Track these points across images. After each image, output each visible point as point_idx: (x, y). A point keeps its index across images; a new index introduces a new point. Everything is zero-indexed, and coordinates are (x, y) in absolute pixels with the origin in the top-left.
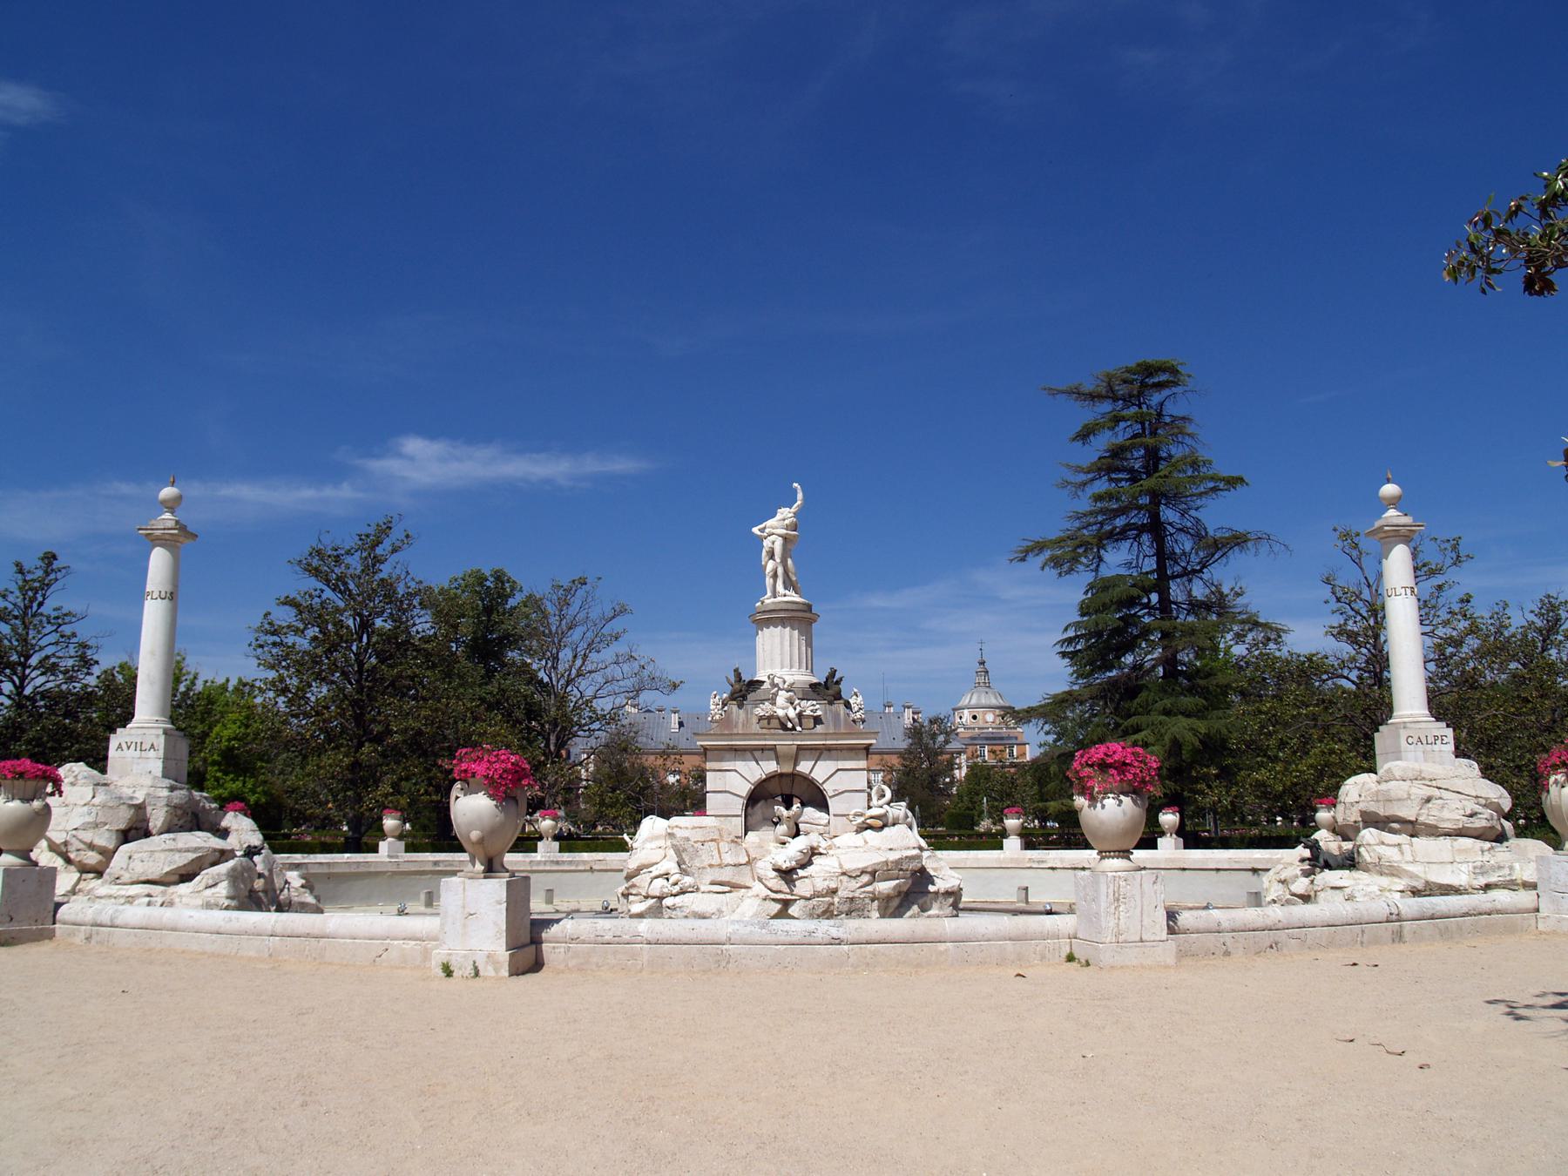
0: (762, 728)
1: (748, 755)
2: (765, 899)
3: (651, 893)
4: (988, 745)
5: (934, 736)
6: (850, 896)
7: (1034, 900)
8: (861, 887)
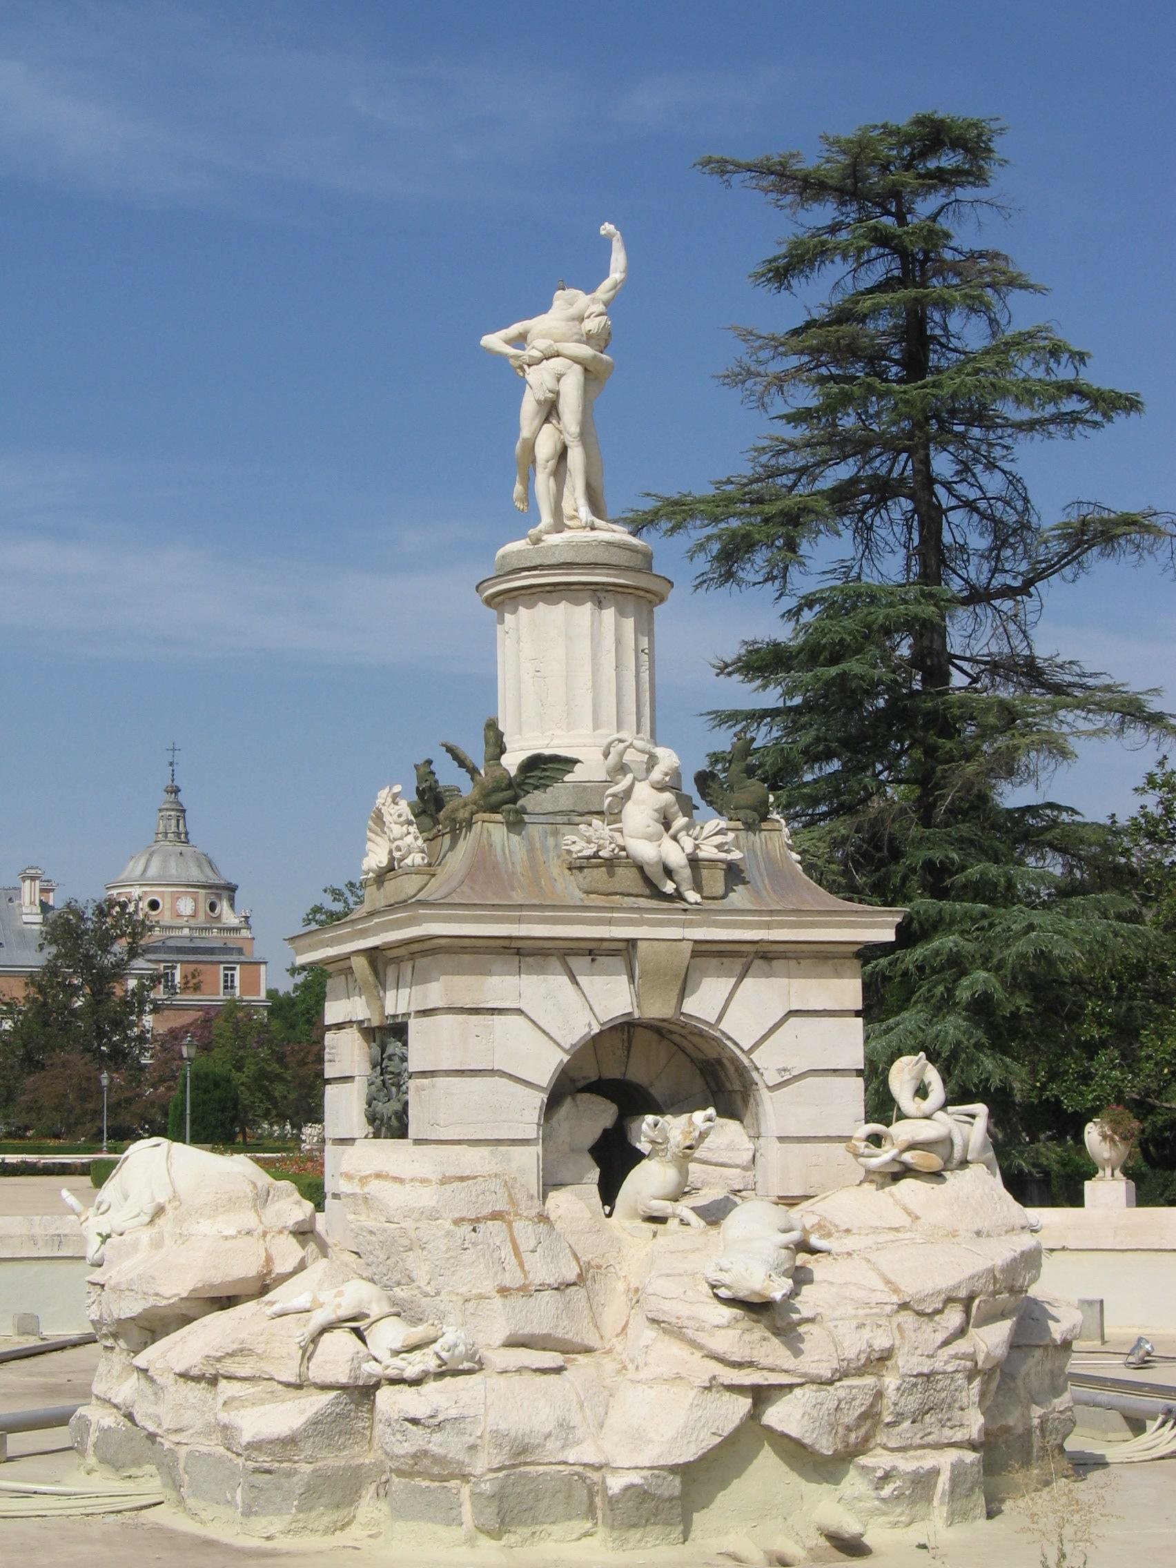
0: (588, 893)
1: (555, 962)
2: (708, 1388)
3: (316, 1372)
4: (181, 962)
5: (105, 941)
6: (926, 1371)
7: (1095, 1342)
8: (946, 1343)
